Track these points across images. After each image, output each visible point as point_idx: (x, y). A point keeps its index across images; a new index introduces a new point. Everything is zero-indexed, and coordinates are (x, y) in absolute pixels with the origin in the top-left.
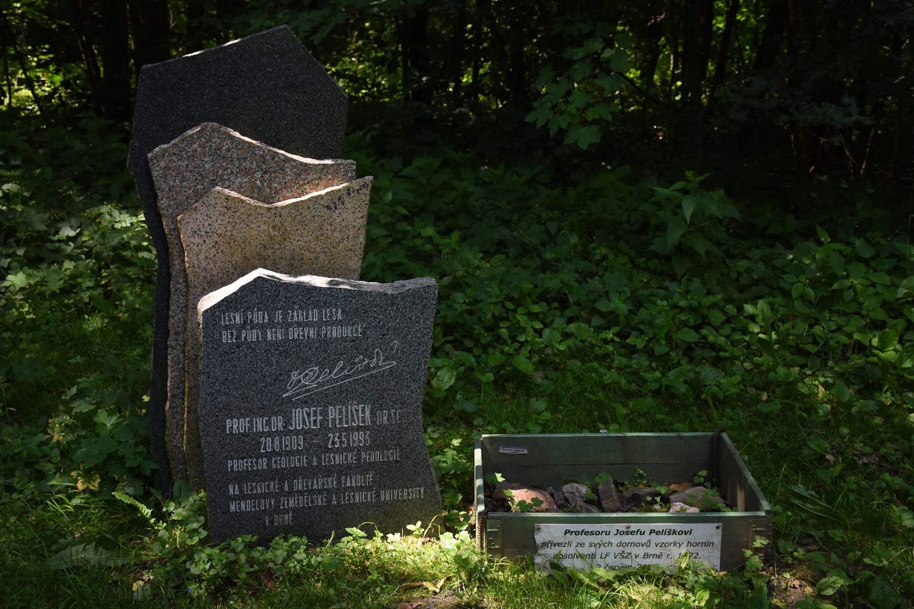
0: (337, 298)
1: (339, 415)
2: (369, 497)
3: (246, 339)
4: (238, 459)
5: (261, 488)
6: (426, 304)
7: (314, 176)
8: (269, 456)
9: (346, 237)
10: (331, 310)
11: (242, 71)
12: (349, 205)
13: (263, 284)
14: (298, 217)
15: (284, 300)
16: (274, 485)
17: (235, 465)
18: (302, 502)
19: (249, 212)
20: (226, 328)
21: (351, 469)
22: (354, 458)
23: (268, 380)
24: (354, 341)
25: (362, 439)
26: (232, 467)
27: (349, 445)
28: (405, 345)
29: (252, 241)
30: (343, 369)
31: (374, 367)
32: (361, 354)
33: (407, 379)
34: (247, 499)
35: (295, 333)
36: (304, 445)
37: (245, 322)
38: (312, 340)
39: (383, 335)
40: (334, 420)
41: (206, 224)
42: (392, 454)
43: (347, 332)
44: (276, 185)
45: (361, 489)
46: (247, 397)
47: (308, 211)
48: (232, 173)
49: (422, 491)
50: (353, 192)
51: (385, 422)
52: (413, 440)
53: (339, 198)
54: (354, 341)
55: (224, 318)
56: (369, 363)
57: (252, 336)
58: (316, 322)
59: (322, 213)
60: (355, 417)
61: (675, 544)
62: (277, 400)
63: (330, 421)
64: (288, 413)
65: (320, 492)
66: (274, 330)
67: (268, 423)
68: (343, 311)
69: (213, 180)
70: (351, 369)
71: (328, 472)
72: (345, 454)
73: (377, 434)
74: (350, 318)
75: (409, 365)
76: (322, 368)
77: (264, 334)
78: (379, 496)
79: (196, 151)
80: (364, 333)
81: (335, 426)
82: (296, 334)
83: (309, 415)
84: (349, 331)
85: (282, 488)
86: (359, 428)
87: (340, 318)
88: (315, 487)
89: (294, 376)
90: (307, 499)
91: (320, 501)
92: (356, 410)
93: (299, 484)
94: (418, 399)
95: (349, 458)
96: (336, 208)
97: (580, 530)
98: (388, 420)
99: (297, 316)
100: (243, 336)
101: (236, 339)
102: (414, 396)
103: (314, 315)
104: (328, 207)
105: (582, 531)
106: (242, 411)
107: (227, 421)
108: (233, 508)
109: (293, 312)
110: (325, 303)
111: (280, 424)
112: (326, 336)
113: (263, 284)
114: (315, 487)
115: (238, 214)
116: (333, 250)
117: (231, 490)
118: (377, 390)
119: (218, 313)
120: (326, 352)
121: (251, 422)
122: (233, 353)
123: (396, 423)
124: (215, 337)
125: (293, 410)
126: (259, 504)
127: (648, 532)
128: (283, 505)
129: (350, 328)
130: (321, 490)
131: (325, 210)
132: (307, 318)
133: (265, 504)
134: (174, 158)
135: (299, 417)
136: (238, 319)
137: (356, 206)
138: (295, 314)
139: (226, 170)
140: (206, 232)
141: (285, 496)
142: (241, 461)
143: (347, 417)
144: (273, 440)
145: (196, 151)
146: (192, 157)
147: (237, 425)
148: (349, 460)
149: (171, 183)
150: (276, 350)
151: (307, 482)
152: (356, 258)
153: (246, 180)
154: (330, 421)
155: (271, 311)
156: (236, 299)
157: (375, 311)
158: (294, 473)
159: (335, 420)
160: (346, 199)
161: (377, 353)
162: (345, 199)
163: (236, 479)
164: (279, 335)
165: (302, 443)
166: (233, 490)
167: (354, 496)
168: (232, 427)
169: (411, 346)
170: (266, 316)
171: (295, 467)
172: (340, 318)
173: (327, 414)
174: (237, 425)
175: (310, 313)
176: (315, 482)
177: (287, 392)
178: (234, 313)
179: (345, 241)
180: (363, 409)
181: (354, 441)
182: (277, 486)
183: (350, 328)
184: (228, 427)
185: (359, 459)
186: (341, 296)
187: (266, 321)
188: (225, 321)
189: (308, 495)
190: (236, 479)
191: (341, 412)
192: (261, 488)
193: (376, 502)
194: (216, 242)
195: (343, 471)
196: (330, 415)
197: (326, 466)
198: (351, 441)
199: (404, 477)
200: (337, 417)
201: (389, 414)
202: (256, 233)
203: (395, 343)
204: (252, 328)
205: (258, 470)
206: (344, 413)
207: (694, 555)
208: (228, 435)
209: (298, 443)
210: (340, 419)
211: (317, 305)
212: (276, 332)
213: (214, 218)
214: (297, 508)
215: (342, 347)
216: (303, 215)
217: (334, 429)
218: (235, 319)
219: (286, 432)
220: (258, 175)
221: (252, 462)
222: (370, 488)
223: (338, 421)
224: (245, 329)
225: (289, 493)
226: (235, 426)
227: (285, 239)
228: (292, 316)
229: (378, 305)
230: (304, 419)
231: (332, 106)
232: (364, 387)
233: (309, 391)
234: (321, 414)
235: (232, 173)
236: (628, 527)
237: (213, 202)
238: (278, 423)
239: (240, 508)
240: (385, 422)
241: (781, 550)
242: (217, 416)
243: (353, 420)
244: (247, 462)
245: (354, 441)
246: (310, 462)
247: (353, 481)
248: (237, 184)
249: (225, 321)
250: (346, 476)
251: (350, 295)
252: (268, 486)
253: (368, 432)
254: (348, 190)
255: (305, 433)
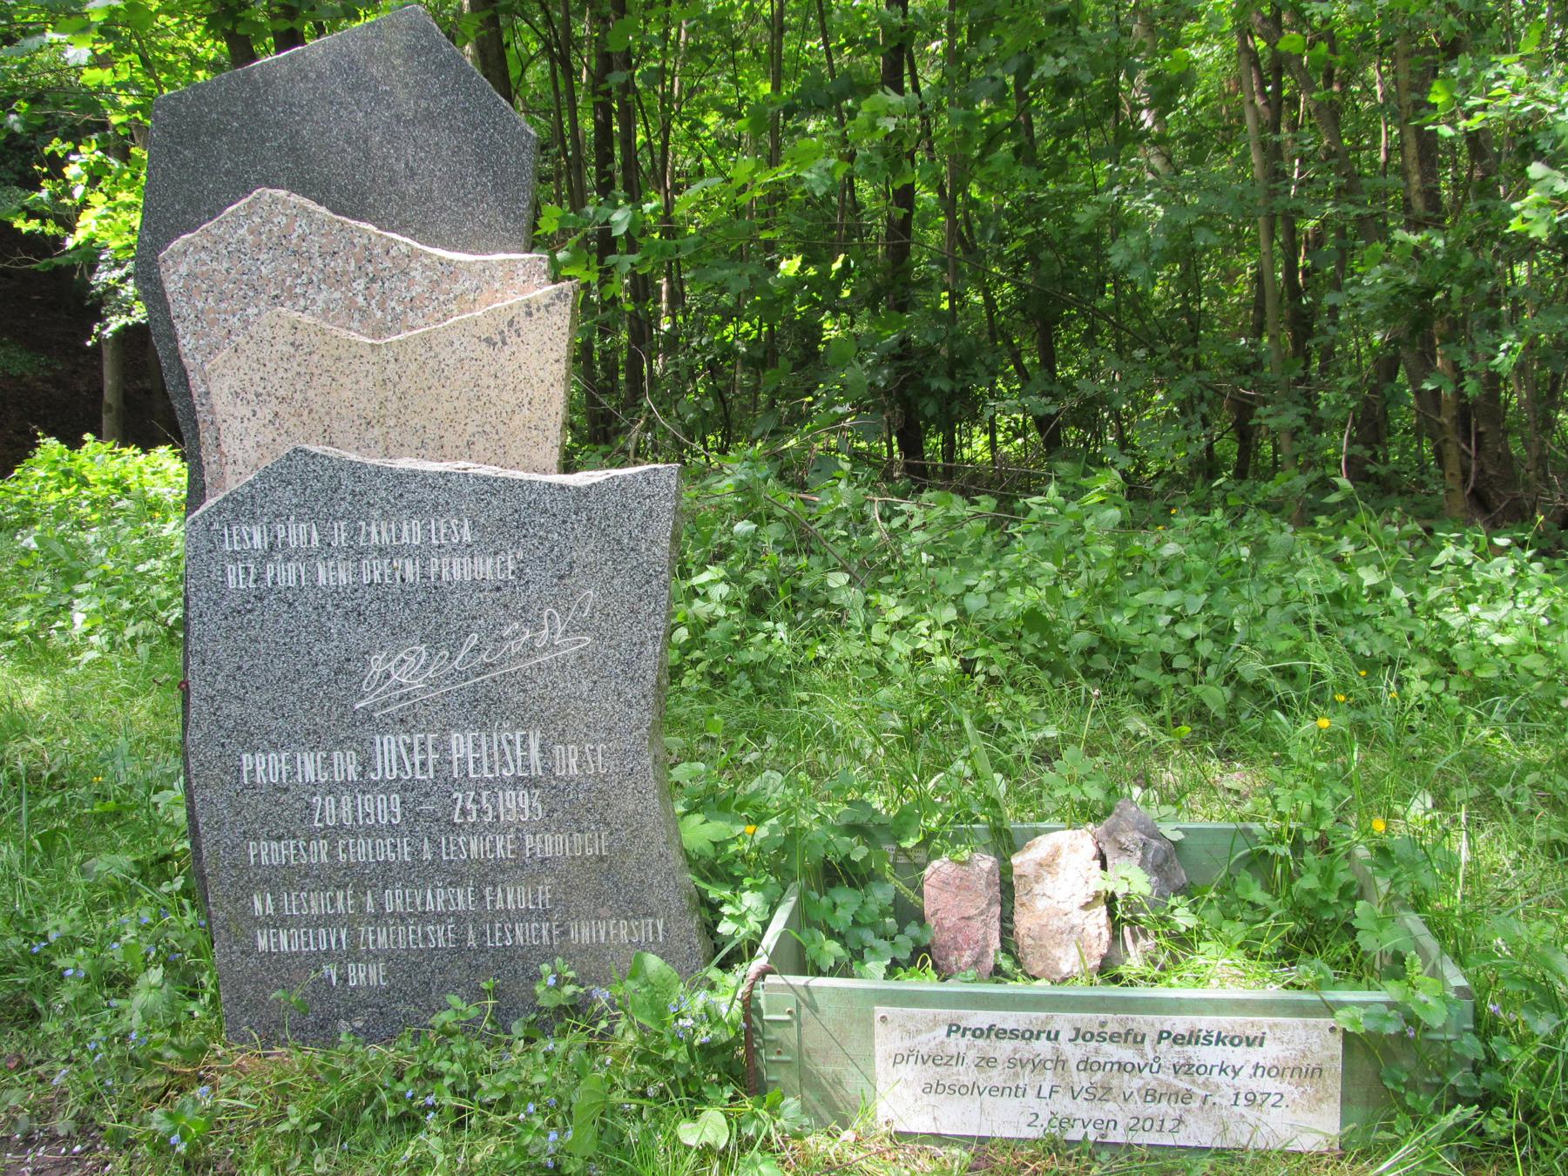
0: (460, 494)
1: (475, 751)
2: (545, 932)
3: (275, 583)
4: (269, 838)
5: (317, 905)
6: (651, 510)
7: (467, 284)
8: (333, 834)
9: (526, 402)
10: (447, 522)
11: (334, 93)
12: (531, 336)
13: (306, 464)
14: (431, 362)
15: (349, 498)
16: (345, 898)
17: (269, 853)
18: (406, 937)
19: (336, 353)
20: (235, 557)
21: (503, 872)
22: (509, 847)
23: (324, 670)
24: (498, 589)
25: (526, 806)
26: (258, 855)
27: (498, 817)
28: (610, 600)
29: (344, 411)
30: (477, 650)
31: (545, 649)
32: (515, 618)
33: (617, 676)
34: (291, 926)
35: (375, 570)
36: (403, 815)
37: (272, 546)
38: (411, 585)
39: (561, 578)
40: (463, 762)
41: (257, 378)
42: (591, 841)
43: (485, 567)
44: (393, 304)
45: (524, 916)
46: (281, 707)
47: (449, 349)
48: (311, 282)
49: (660, 927)
50: (538, 310)
51: (574, 771)
52: (635, 811)
53: (511, 323)
54: (498, 589)
55: (231, 536)
56: (533, 638)
57: (286, 574)
58: (419, 547)
59: (477, 354)
60: (509, 757)
61: (1222, 1070)
62: (342, 716)
63: (455, 764)
64: (367, 744)
65: (440, 918)
66: (331, 564)
67: (328, 763)
68: (474, 525)
69: (276, 296)
70: (495, 650)
71: (456, 878)
72: (490, 837)
73: (556, 796)
74: (490, 538)
75: (619, 645)
76: (434, 647)
77: (312, 573)
78: (566, 933)
79: (243, 241)
80: (519, 574)
81: (467, 775)
82: (377, 573)
83: (410, 749)
84: (488, 567)
85: (361, 907)
86: (518, 782)
87: (468, 538)
88: (430, 907)
89: (377, 665)
90: (415, 932)
91: (440, 936)
92: (509, 742)
93: (394, 900)
94: (641, 721)
95: (499, 846)
96: (504, 343)
97: (985, 1027)
98: (579, 766)
99: (378, 533)
100: (269, 575)
101: (255, 581)
102: (634, 714)
103: (412, 532)
104: (489, 341)
105: (990, 1028)
106: (273, 737)
107: (244, 757)
108: (262, 943)
109: (368, 525)
110: (435, 506)
111: (351, 769)
112: (440, 578)
113: (306, 464)
114: (430, 907)
115: (316, 357)
116: (501, 426)
117: (258, 905)
118: (552, 699)
119: (216, 526)
120: (438, 611)
121: (291, 761)
122: (250, 611)
123: (597, 772)
124: (213, 577)
125: (377, 738)
126: (316, 939)
127: (1152, 1036)
128: (366, 943)
129: (490, 561)
130: (440, 915)
131: (484, 345)
132: (398, 539)
133: (325, 939)
134: (203, 255)
135: (388, 747)
136: (257, 537)
137: (546, 338)
138: (374, 530)
139: (298, 276)
140: (258, 395)
141: (369, 923)
142: (274, 845)
143: (490, 756)
144: (338, 801)
145: (243, 241)
146: (237, 253)
147: (263, 766)
148: (500, 851)
149: (200, 305)
150: (338, 606)
151: (412, 896)
152: (549, 445)
153: (337, 295)
154: (455, 764)
155: (324, 521)
156: (253, 497)
157: (541, 525)
158: (384, 875)
159: (466, 763)
160: (525, 324)
161: (551, 614)
162: (522, 324)
163: (267, 881)
164: (342, 575)
165: (398, 811)
166: (261, 905)
167: (512, 931)
168: (254, 770)
169: (622, 603)
170: (315, 534)
171: (386, 861)
172: (468, 538)
173: (447, 750)
174: (263, 766)
175: (405, 528)
176: (429, 896)
177: (363, 697)
178: (250, 525)
179: (525, 410)
180: (525, 738)
181: (508, 811)
182: (350, 902)
183: (490, 561)
184: (245, 769)
185: (518, 851)
186: (467, 490)
187: (315, 542)
188: (231, 543)
189: (415, 924)
190: (267, 881)
191: (477, 746)
192: (317, 905)
193: (561, 946)
194: (276, 414)
195: (489, 874)
196: (454, 750)
197: (451, 862)
198: (502, 810)
199: (619, 891)
200: (471, 756)
201: (581, 753)
202: (350, 394)
203: (587, 597)
204: (288, 559)
205: (309, 866)
206: (485, 748)
207: (1272, 1099)
208: (246, 787)
209: (387, 809)
210: (476, 760)
211: (417, 509)
212: (335, 568)
213: (271, 366)
214: (393, 951)
215: (474, 601)
216: (441, 357)
217: (463, 782)
218: (251, 539)
219: (364, 785)
220: (360, 285)
221: (297, 847)
222: (545, 915)
223: (471, 766)
224: (275, 562)
225: (376, 917)
226: (260, 770)
227: (406, 407)
228: (368, 534)
229: (546, 511)
230: (400, 757)
231: (504, 153)
232: (525, 691)
233: (408, 697)
234: (435, 748)
235: (311, 282)
236: (1103, 1024)
237: (268, 334)
238: (346, 765)
239: (277, 944)
240: (574, 771)
241: (224, 448)
242: (223, 745)
243: (505, 764)
244: (287, 847)
245: (508, 811)
246: (417, 853)
247: (510, 898)
248: (320, 303)
249: (231, 543)
250: (495, 886)
251: (486, 487)
252: (333, 901)
253: (538, 792)
254: (528, 306)
255: (405, 788)
